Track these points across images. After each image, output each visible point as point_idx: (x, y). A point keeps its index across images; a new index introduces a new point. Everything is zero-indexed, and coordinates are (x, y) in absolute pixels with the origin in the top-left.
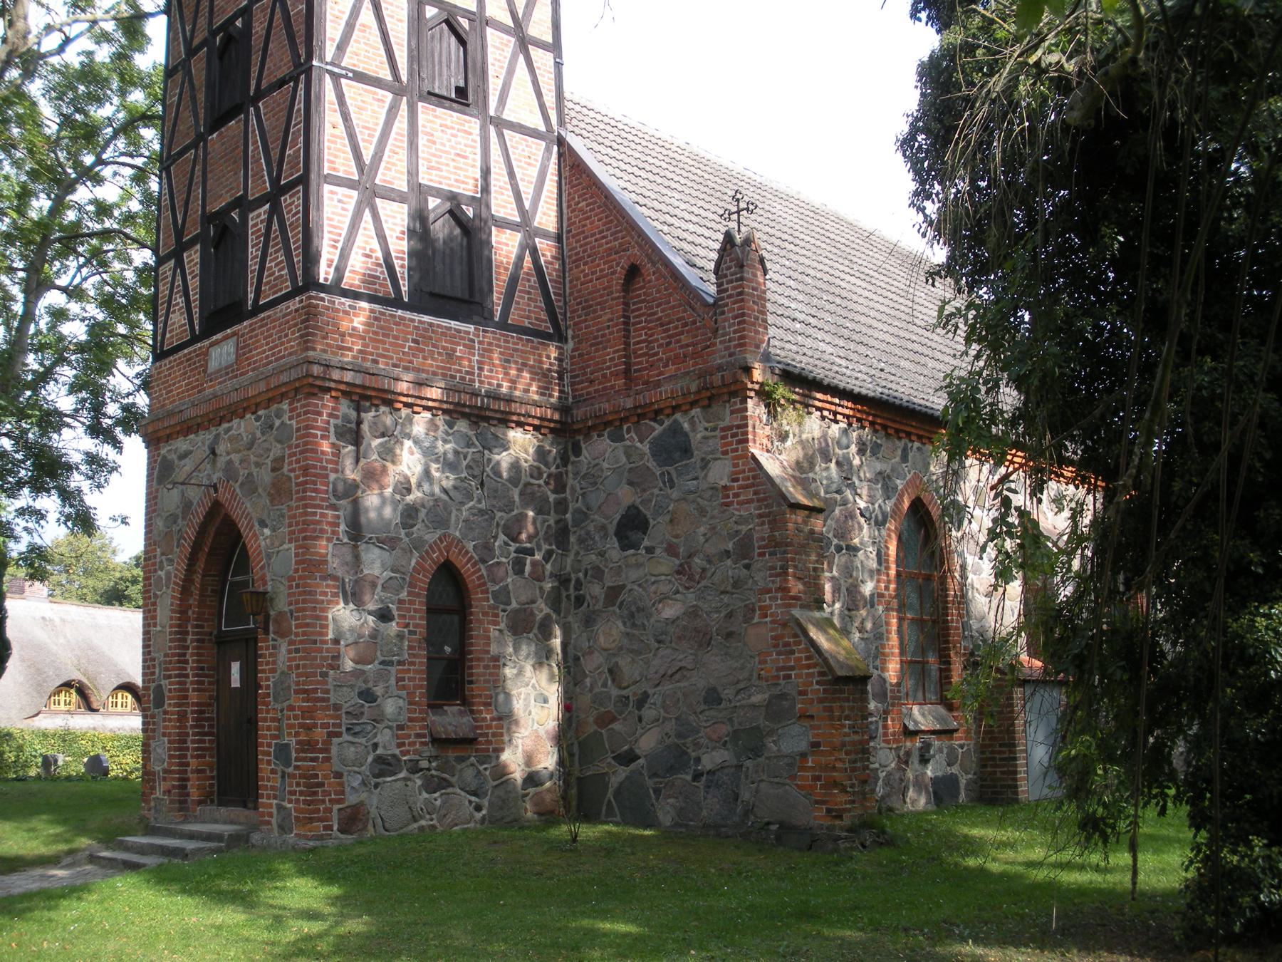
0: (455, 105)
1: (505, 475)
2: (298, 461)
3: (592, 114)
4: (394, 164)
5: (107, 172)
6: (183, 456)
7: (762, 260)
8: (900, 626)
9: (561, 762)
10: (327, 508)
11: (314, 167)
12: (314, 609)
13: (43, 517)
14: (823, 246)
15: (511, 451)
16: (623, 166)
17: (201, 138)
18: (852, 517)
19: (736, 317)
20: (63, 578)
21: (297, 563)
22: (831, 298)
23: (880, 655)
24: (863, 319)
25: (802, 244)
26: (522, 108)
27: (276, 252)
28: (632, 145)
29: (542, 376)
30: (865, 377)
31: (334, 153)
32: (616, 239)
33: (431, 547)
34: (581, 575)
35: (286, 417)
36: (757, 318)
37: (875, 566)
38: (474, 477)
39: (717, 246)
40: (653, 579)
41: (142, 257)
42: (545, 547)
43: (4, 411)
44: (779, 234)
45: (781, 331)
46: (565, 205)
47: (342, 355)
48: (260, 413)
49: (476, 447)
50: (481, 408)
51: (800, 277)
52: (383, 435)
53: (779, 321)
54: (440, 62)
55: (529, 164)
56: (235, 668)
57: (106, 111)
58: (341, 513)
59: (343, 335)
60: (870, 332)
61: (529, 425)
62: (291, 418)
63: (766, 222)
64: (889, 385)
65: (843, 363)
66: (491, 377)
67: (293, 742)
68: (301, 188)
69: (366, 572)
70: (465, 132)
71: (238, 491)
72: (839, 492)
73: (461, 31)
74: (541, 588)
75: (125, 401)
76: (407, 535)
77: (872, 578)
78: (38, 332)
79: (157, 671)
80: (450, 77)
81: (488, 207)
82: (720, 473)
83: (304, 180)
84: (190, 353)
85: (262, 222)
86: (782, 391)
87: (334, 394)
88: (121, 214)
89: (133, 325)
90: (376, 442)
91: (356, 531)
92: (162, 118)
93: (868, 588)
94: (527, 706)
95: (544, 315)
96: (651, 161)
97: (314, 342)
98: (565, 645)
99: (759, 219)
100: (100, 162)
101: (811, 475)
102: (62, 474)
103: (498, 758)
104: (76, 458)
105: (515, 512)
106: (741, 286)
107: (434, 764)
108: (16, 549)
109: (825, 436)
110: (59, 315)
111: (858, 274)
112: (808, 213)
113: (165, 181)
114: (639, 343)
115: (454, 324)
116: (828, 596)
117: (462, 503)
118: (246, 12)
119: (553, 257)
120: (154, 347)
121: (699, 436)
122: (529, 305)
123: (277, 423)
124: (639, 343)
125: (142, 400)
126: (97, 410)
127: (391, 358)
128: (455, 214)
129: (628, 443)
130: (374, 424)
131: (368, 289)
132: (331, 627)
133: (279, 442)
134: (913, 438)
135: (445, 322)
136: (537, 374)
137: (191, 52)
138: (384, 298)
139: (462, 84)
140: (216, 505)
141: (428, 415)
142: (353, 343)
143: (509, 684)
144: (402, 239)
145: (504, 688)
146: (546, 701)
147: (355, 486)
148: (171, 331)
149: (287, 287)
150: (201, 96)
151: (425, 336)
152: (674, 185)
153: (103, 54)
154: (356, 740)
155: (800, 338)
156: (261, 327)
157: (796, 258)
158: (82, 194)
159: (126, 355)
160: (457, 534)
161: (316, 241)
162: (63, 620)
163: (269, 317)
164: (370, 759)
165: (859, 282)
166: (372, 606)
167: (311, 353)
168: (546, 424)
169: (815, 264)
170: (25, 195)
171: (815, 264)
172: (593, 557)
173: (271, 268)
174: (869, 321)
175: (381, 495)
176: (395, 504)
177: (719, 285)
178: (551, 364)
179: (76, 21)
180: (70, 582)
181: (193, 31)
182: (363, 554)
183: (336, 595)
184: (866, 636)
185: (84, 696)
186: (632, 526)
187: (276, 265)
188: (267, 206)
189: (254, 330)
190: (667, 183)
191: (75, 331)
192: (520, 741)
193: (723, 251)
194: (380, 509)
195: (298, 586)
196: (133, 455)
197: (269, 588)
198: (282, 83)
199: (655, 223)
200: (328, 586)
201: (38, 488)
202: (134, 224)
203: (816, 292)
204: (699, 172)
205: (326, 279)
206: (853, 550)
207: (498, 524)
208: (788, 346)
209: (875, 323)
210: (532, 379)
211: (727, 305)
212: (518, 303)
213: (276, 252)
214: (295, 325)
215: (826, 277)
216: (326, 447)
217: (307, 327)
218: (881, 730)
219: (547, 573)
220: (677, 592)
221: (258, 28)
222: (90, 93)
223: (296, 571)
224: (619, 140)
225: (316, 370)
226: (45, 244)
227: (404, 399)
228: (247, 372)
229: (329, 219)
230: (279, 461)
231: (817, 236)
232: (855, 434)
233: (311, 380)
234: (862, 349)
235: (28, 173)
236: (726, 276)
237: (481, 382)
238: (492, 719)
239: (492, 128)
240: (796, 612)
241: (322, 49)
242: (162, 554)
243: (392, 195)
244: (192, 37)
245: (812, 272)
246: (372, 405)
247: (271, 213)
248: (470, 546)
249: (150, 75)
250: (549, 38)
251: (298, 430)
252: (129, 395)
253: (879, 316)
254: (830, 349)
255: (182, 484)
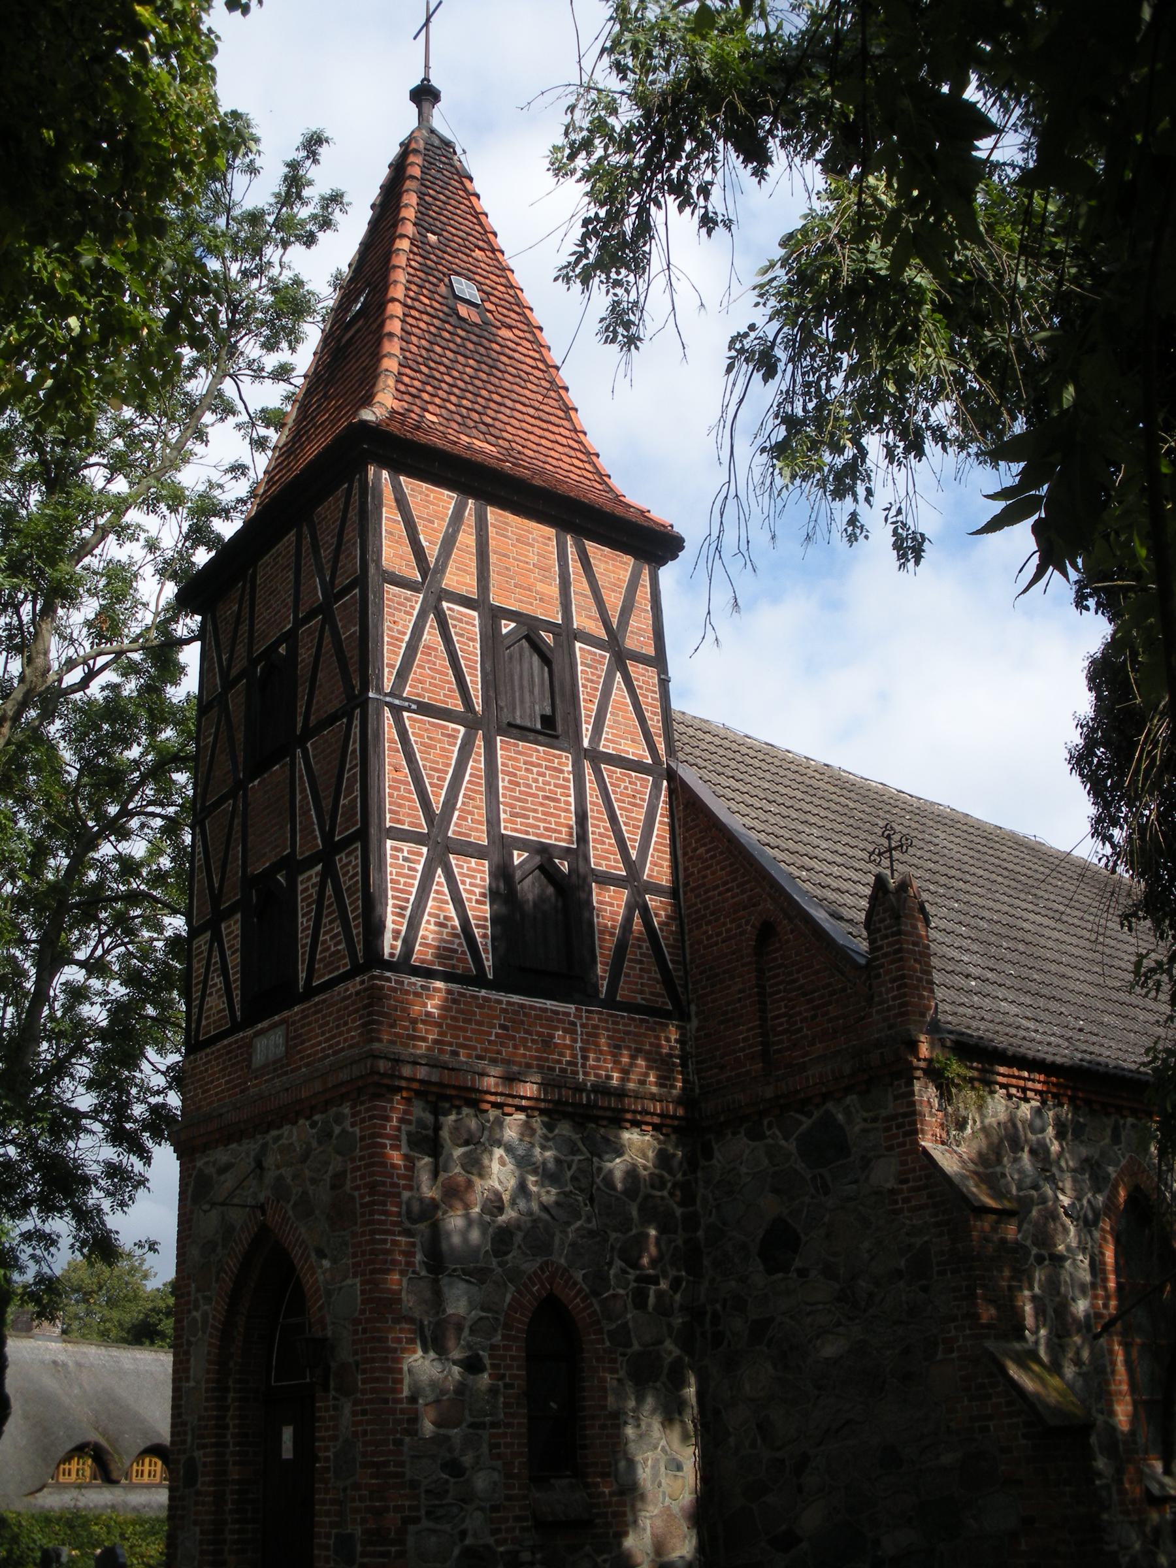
0: (541, 738)
1: (619, 1186)
2: (362, 1177)
3: (708, 738)
4: (471, 813)
5: (134, 823)
6: (227, 1168)
7: (922, 909)
8: (1127, 1354)
9: (701, 1548)
10: (400, 1234)
11: (374, 820)
12: (386, 1359)
13: (54, 1243)
14: (1000, 879)
15: (626, 1157)
16: (750, 801)
17: (240, 785)
18: (1054, 1217)
19: (893, 981)
20: (81, 1309)
21: (363, 1302)
22: (1012, 944)
23: (1102, 1395)
24: (1053, 967)
25: (973, 880)
26: (622, 737)
27: (331, 922)
28: (760, 774)
29: (661, 1064)
30: (1060, 1041)
31: (398, 804)
32: (743, 892)
33: (530, 1278)
34: (718, 1307)
35: (347, 1124)
36: (920, 980)
37: (1088, 1278)
38: (582, 1190)
39: (868, 891)
40: (809, 1308)
41: (176, 924)
42: (673, 1273)
43: (10, 1113)
44: (944, 870)
45: (952, 992)
46: (680, 853)
47: (415, 1046)
48: (316, 1117)
49: (582, 1154)
50: (588, 1105)
51: (973, 922)
52: (467, 1143)
53: (950, 980)
54: (521, 687)
55: (635, 805)
56: (287, 1434)
57: (134, 752)
58: (417, 1240)
59: (414, 1021)
60: (1063, 982)
61: (647, 1124)
62: (353, 1125)
63: (927, 856)
64: (1092, 1048)
65: (1031, 1025)
66: (599, 1068)
67: (358, 1532)
68: (358, 844)
69: (450, 1311)
70: (555, 769)
71: (290, 1213)
72: (1036, 1187)
73: (544, 648)
74: (669, 1325)
75: (153, 1100)
76: (500, 1264)
77: (1084, 1293)
78: (52, 1018)
79: (189, 1439)
80: (533, 703)
81: (587, 859)
82: (884, 1174)
83: (363, 836)
84: (230, 1044)
85: (314, 886)
86: (956, 1069)
87: (405, 1094)
88: (149, 873)
89: (164, 1006)
90: (458, 1152)
91: (438, 1259)
92: (195, 758)
93: (1081, 1306)
94: (655, 1475)
95: (659, 988)
96: (784, 791)
97: (378, 1031)
98: (700, 1394)
99: (919, 853)
100: (125, 813)
101: (998, 1169)
102: (77, 1190)
103: (620, 1544)
104: (94, 1170)
105: (634, 1232)
106: (898, 942)
107: (538, 1556)
108: (25, 1278)
109: (1012, 1119)
110: (78, 994)
111: (1043, 912)
112: (979, 840)
113: (198, 837)
114: (777, 1017)
115: (550, 1004)
116: (1029, 1321)
117: (568, 1224)
118: (290, 637)
119: (667, 916)
120: (188, 1030)
121: (857, 1129)
122: (641, 977)
123: (337, 1130)
124: (777, 1017)
125: (174, 1100)
126: (121, 1110)
127: (475, 1048)
128: (547, 870)
129: (770, 1141)
130: (456, 1129)
131: (444, 965)
132: (406, 1381)
133: (339, 1153)
134: (1126, 1112)
135: (539, 1003)
136: (655, 1061)
137: (229, 684)
138: (458, 966)
139: (548, 711)
140: (264, 1229)
141: (521, 1116)
142: (427, 1031)
143: (632, 1447)
144: (483, 903)
145: (625, 1453)
146: (679, 1468)
147: (434, 1205)
148: (207, 1018)
149: (345, 966)
150: (240, 736)
151: (516, 1019)
152: (813, 820)
153: (130, 687)
154: (438, 1527)
155: (976, 998)
156: (316, 1012)
157: (967, 897)
158: (106, 849)
159: (156, 1042)
160: (562, 1261)
161: (379, 908)
162: (79, 1365)
163: (324, 1001)
164: (456, 1551)
165: (1046, 921)
166: (456, 1355)
167: (376, 1045)
168: (668, 1121)
169: (991, 904)
170: (40, 852)
171: (991, 904)
172: (733, 1284)
173: (325, 942)
174: (1062, 969)
175: (467, 1216)
176: (484, 1227)
177: (872, 942)
178: (671, 1048)
179: (100, 654)
180: (89, 1313)
181: (230, 660)
182: (445, 1289)
183: (412, 1341)
184: (1085, 1369)
185: (104, 1468)
186: (779, 1245)
187: (332, 938)
188: (320, 867)
189: (307, 1016)
190: (803, 817)
191: (95, 1013)
192: (648, 1522)
193: (873, 899)
194: (464, 1233)
195: (364, 1331)
196: (164, 1165)
197: (329, 1334)
198: (333, 719)
199: (792, 869)
200: (401, 1330)
201: (48, 1208)
202: (165, 884)
203: (993, 939)
204: (842, 800)
205: (392, 955)
206: (1058, 1260)
207: (613, 1248)
208: (961, 1010)
209: (1069, 972)
210: (648, 1068)
211: (882, 966)
212: (627, 975)
213: (331, 922)
214: (356, 1011)
215: (1006, 919)
216: (396, 1157)
217: (370, 1014)
218: (1115, 1497)
219: (676, 1306)
220: (839, 1324)
221: (305, 655)
222: (114, 733)
223: (363, 1312)
224: (743, 768)
225: (382, 1065)
226: (61, 910)
227: (492, 1098)
228: (300, 1068)
229: (392, 881)
230: (339, 1177)
231: (992, 868)
232: (1051, 1114)
233: (376, 1078)
234: (1053, 1006)
235: (44, 826)
236: (879, 930)
237: (586, 1074)
238: (612, 1494)
239: (587, 763)
240: (990, 1345)
241: (380, 677)
242: (198, 1290)
243: (468, 850)
244: (229, 667)
245: (986, 914)
246: (453, 1106)
247: (323, 876)
248: (579, 1275)
249: (182, 710)
250: (651, 651)
251: (362, 1139)
252: (158, 1093)
253: (1073, 961)
254: (1014, 1009)
255: (223, 1204)
